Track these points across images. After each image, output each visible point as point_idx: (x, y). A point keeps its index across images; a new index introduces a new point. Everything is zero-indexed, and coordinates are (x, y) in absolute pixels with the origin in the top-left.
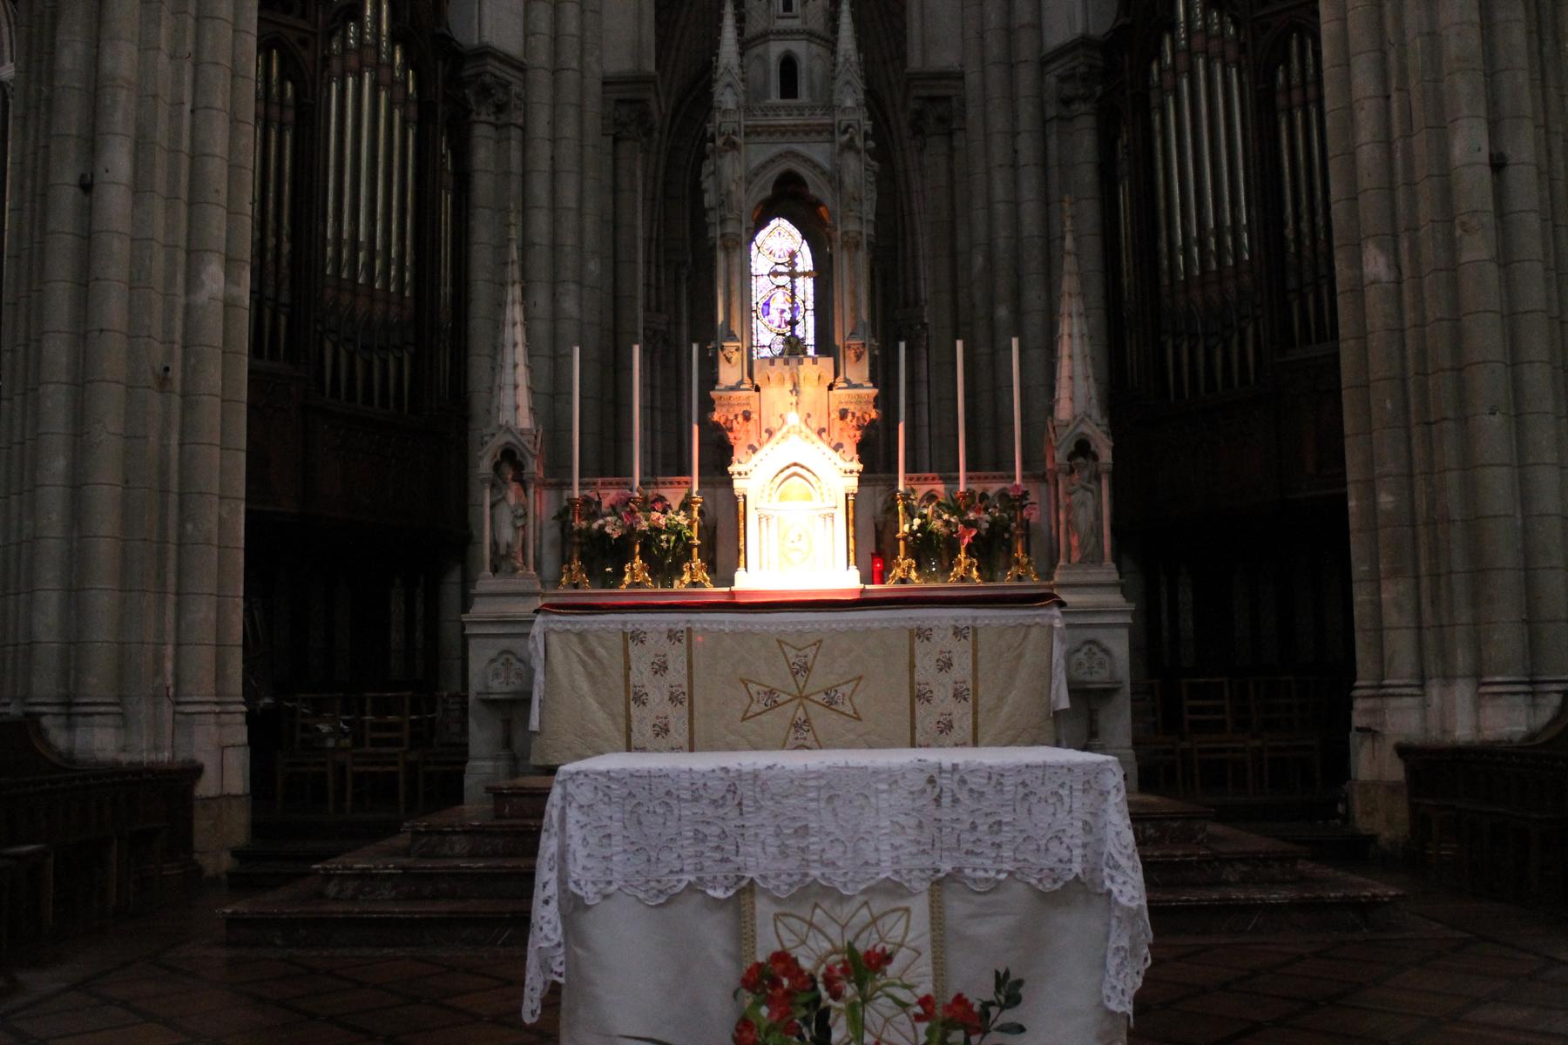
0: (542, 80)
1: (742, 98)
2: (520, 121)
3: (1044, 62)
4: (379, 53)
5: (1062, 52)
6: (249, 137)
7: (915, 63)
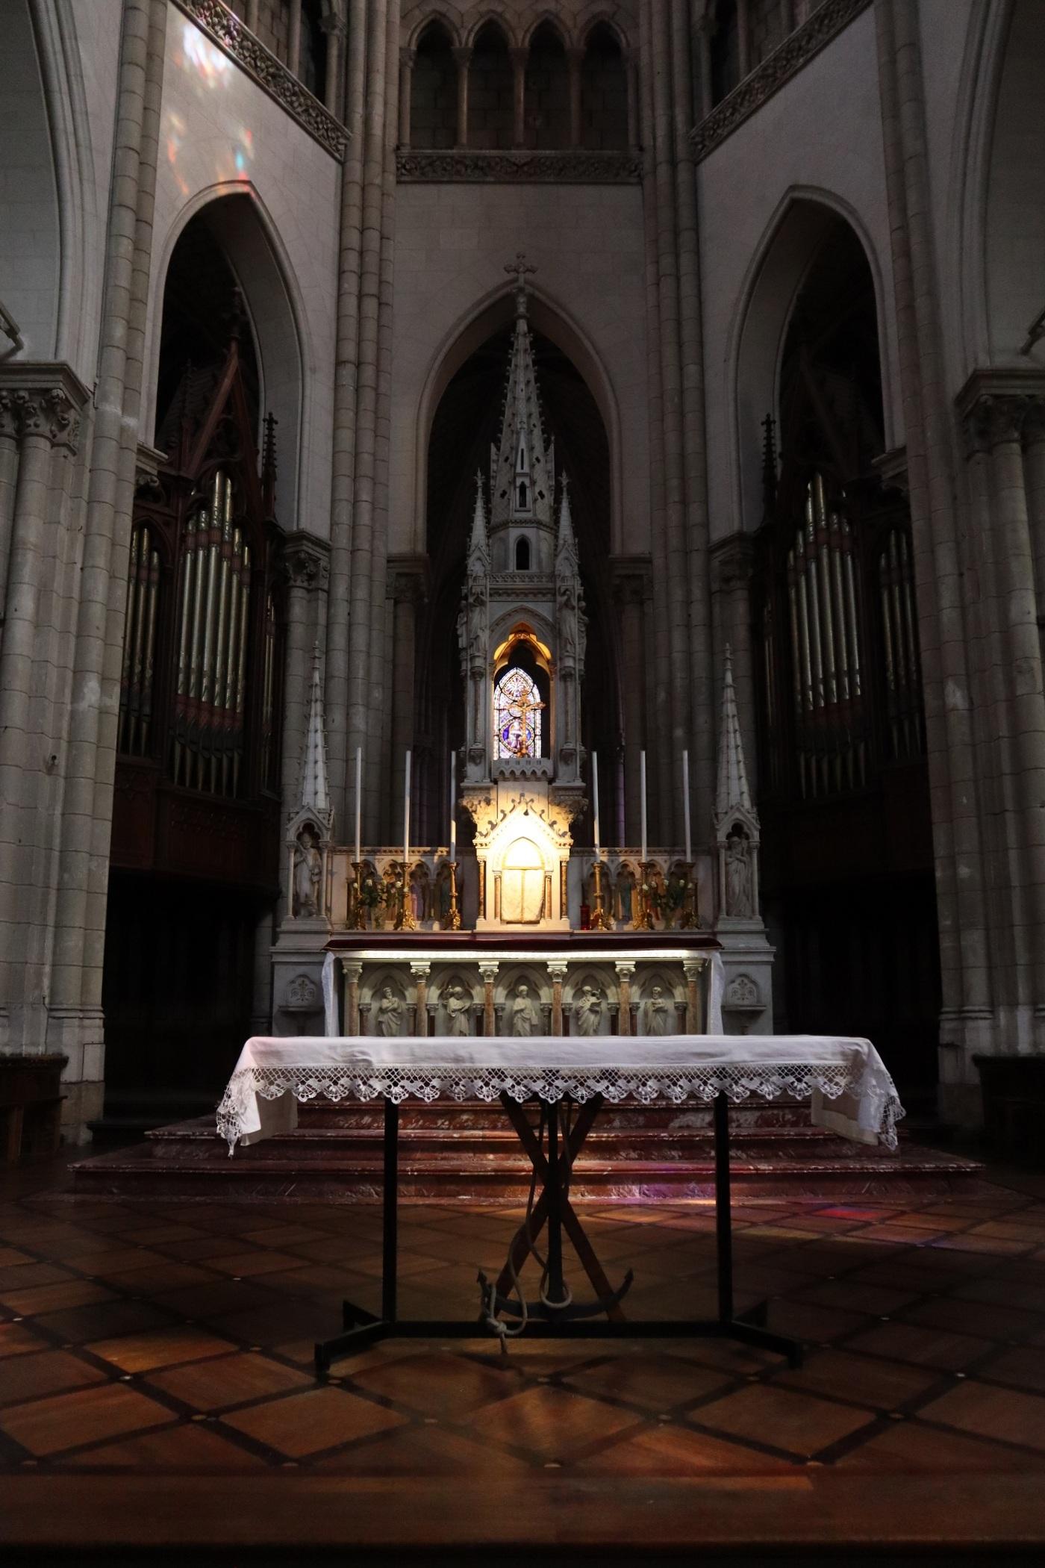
0: (342, 560)
1: (489, 568)
2: (326, 587)
3: (711, 550)
4: (223, 534)
5: (724, 543)
6: (121, 590)
7: (617, 550)
